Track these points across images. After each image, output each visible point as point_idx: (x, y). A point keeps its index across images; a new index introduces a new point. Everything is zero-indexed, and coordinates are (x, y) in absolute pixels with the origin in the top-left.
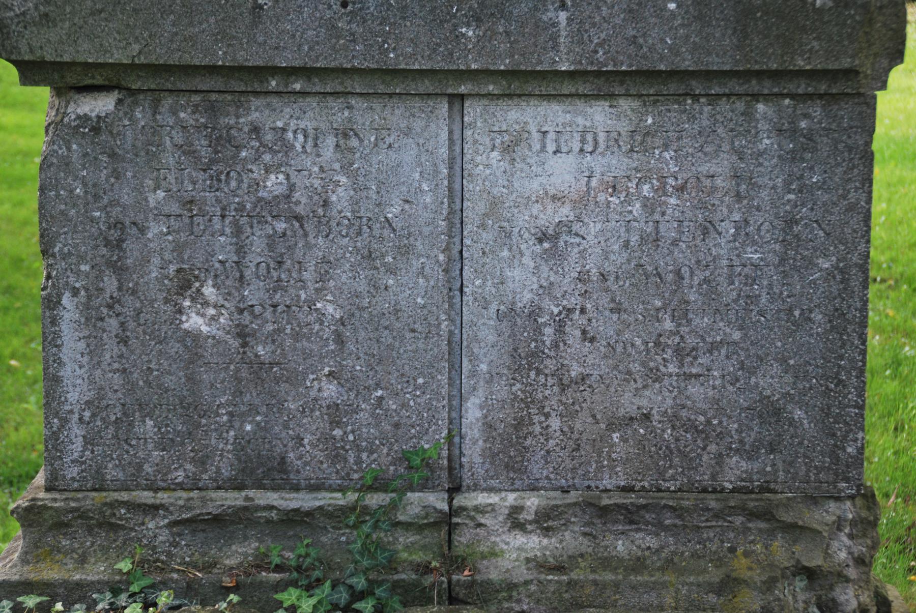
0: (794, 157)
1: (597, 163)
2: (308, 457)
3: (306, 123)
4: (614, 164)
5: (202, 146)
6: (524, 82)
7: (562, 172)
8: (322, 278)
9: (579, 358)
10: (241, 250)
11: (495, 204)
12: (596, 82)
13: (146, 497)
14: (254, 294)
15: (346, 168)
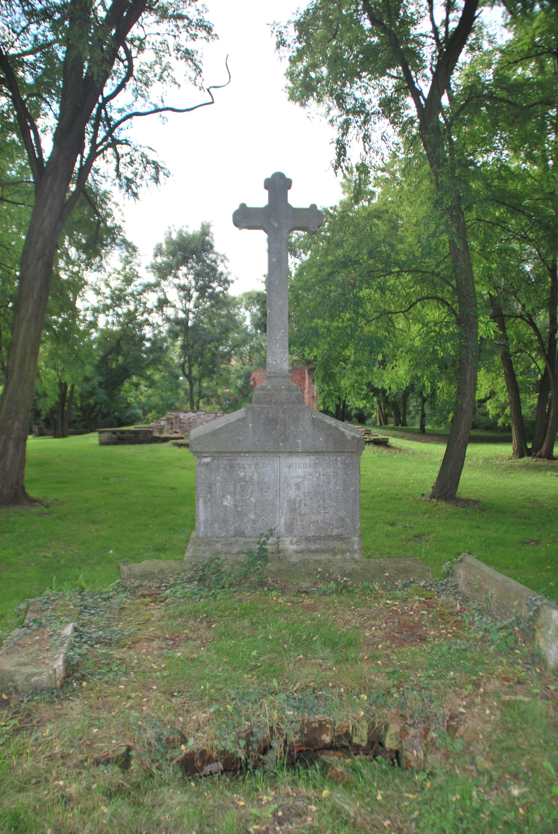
0: (345, 468)
1: (307, 470)
2: (248, 531)
3: (249, 463)
4: (310, 470)
5: (228, 467)
6: (292, 453)
7: (300, 472)
8: (252, 494)
9: (304, 509)
10: (235, 488)
11: (286, 478)
12: (307, 453)
13: (216, 539)
14: (237, 497)
15: (257, 471)
